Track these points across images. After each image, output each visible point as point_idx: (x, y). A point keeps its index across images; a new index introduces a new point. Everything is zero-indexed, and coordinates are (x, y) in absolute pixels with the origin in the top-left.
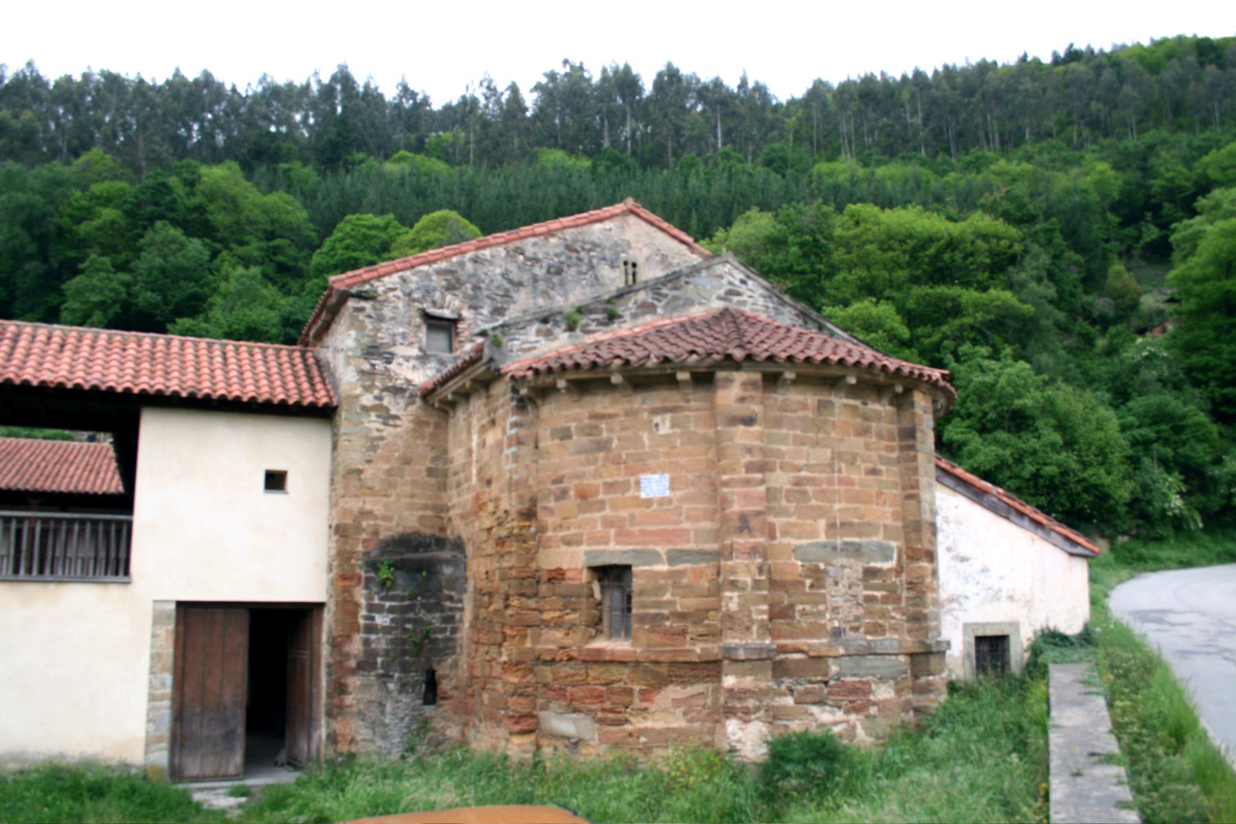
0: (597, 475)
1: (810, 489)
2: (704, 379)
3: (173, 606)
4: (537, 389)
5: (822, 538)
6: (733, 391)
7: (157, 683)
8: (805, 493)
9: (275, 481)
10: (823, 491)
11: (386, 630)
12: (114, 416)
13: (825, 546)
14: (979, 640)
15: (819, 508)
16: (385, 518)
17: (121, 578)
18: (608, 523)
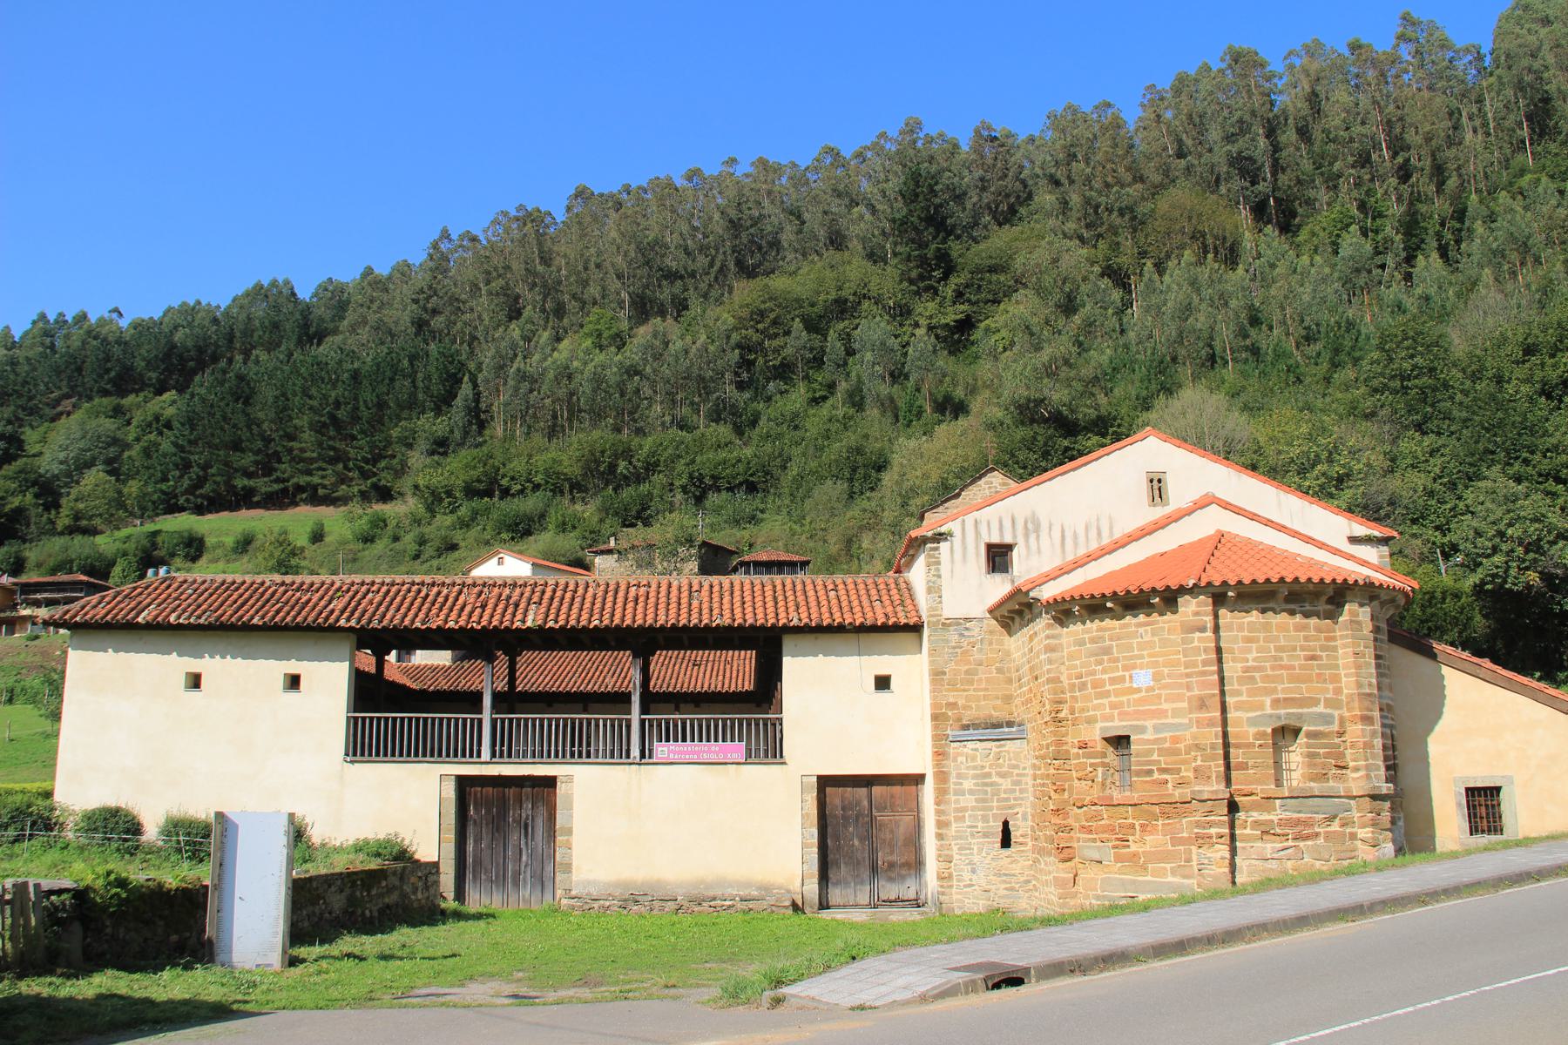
0: (1104, 671)
1: (1257, 675)
2: (1170, 598)
4: (1063, 611)
5: (1269, 711)
6: (1190, 607)
7: (807, 835)
8: (1253, 678)
9: (883, 683)
11: (971, 792)
12: (767, 645)
13: (1271, 716)
14: (1467, 789)
16: (965, 707)
17: (778, 760)
18: (1113, 706)
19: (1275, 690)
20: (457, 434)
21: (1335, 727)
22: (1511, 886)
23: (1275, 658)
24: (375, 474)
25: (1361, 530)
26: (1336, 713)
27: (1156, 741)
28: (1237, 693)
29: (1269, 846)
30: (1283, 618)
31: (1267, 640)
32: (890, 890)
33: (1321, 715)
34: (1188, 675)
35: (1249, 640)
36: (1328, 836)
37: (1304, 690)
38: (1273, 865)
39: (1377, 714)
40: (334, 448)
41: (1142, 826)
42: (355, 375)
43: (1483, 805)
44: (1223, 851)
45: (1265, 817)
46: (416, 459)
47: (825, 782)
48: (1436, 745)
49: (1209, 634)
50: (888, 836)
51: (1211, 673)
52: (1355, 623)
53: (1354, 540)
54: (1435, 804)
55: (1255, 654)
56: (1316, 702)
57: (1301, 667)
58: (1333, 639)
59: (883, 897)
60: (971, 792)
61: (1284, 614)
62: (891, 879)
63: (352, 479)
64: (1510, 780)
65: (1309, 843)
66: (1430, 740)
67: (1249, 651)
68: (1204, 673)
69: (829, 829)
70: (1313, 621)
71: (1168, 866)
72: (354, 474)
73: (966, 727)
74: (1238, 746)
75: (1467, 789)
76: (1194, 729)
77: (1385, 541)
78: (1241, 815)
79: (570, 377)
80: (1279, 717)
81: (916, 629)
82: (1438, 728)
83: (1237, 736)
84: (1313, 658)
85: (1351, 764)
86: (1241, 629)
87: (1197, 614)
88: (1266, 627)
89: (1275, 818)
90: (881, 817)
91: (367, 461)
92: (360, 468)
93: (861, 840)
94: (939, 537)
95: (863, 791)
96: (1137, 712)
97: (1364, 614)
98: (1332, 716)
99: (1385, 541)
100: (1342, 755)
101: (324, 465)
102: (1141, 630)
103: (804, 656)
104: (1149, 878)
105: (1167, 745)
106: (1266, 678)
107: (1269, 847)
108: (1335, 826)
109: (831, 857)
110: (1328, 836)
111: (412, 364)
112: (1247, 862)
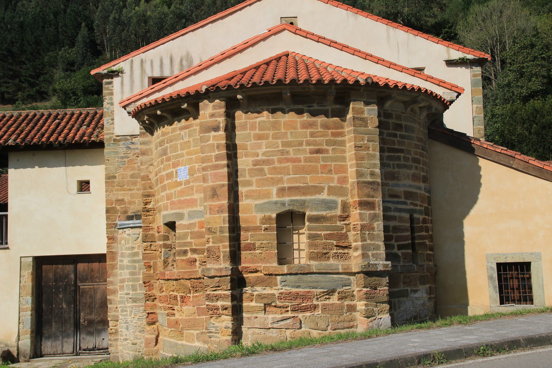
1: (266, 168)
3: (31, 259)
5: (275, 198)
6: (211, 111)
8: (262, 170)
10: (275, 168)
11: (128, 267)
13: (276, 203)
14: (499, 265)
15: (272, 178)
16: (130, 203)
19: (281, 180)
20: (79, 59)
21: (338, 212)
22: (509, 351)
23: (282, 152)
24: (38, 84)
25: (456, 54)
26: (339, 200)
27: (190, 226)
28: (249, 183)
29: (270, 316)
30: (291, 117)
31: (275, 137)
32: (88, 342)
33: (323, 202)
34: (204, 169)
35: (259, 137)
36: (325, 308)
37: (309, 180)
38: (273, 333)
39: (378, 200)
40: (11, 70)
41: (182, 297)
42: (22, 25)
43: (514, 279)
44: (227, 321)
45: (268, 291)
46: (58, 73)
47: (40, 262)
48: (472, 227)
49: (222, 133)
50: (89, 300)
51: (222, 167)
52: (360, 121)
53: (450, 63)
54: (469, 276)
55: (264, 150)
56: (320, 190)
57: (306, 160)
58: (342, 134)
59: (84, 346)
60: (128, 267)
61: (292, 114)
62: (90, 333)
63: (25, 88)
64: (538, 256)
65: (308, 314)
66: (467, 222)
67: (260, 147)
68: (216, 167)
69: (44, 296)
70: (321, 119)
71: (195, 332)
72: (25, 85)
73: (130, 218)
74: (247, 230)
75: (499, 265)
76: (208, 215)
77: (479, 62)
78: (248, 290)
79: (146, 22)
80: (283, 204)
81: (100, 145)
82: (473, 212)
83: (246, 221)
84: (318, 151)
85: (354, 244)
86: (253, 127)
87: (212, 115)
88: (275, 126)
89: (276, 293)
90: (83, 286)
91: (31, 76)
92: (28, 81)
93: (68, 304)
94: (113, 74)
95: (70, 267)
96: (180, 202)
97: (371, 112)
98: (335, 202)
99: (479, 62)
100: (346, 236)
101: (8, 80)
102: (183, 133)
103: (24, 167)
104: (184, 342)
105: (196, 229)
106: (274, 170)
107: (271, 317)
108: (334, 299)
109: (45, 317)
110: (325, 308)
111: (56, 18)
112: (251, 331)
